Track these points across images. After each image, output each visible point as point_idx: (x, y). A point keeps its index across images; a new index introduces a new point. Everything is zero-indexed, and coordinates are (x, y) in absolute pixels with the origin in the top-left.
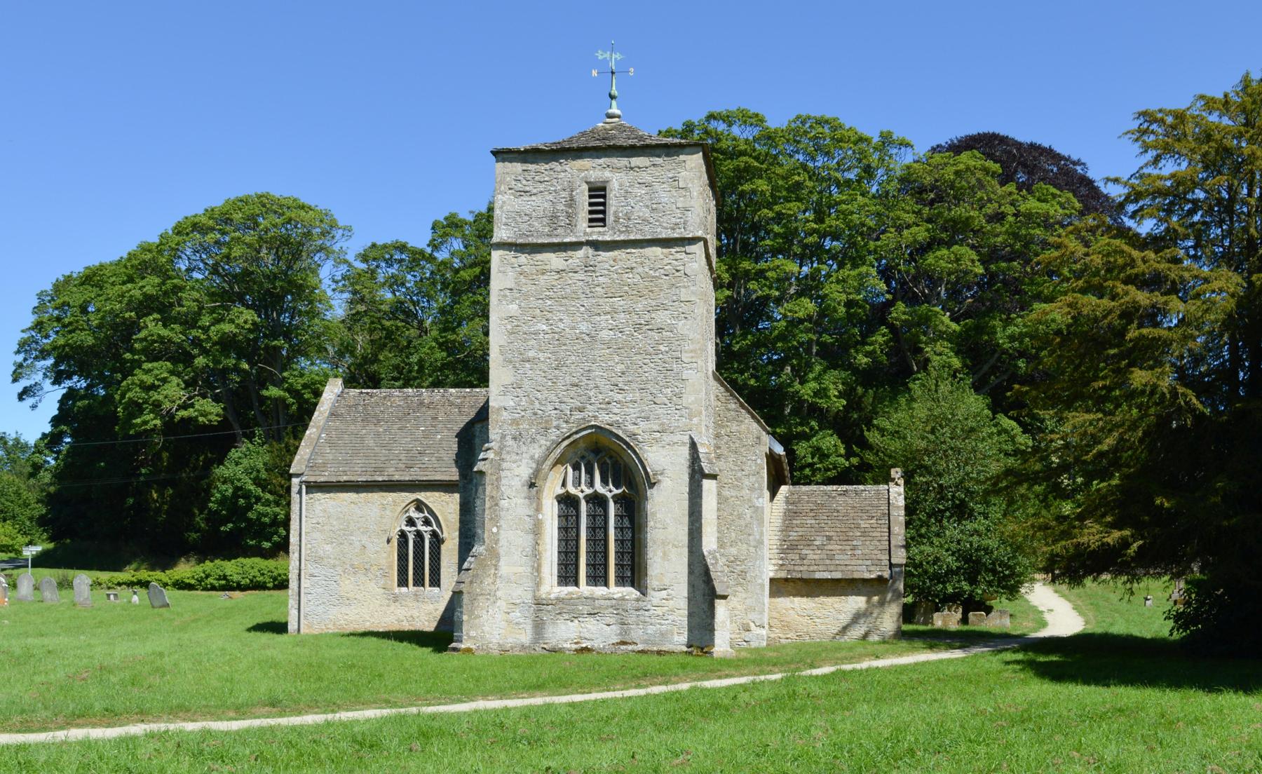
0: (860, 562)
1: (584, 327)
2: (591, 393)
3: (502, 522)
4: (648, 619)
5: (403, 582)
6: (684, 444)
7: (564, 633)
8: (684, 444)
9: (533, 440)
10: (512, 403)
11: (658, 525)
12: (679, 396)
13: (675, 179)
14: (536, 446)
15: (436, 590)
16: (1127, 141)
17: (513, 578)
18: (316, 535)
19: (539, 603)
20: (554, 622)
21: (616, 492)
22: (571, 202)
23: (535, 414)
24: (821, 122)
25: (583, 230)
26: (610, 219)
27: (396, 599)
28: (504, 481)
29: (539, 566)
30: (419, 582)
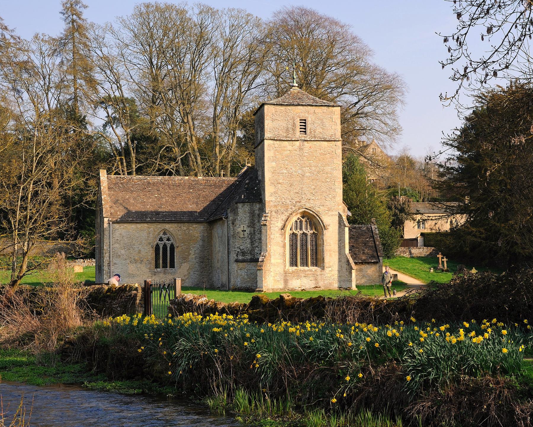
1: (300, 172)
5: (157, 266)
9: (283, 213)
12: (334, 197)
14: (284, 215)
18: (117, 245)
22: (294, 125)
25: (298, 134)
26: (308, 131)
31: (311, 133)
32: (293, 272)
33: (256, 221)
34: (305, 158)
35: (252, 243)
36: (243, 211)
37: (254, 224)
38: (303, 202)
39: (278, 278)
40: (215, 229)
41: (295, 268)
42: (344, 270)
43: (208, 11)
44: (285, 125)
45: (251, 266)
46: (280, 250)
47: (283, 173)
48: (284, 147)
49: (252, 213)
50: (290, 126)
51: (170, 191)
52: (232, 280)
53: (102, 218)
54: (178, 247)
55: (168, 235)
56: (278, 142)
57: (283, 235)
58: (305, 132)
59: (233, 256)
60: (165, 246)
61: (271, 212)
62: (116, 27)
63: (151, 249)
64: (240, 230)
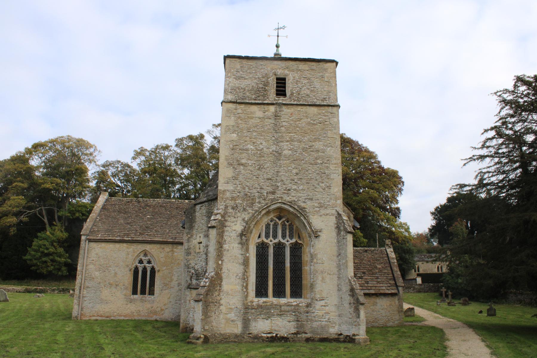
0: (382, 285)
2: (279, 184)
3: (224, 258)
4: (313, 319)
5: (135, 292)
6: (333, 215)
7: (261, 326)
8: (333, 215)
9: (244, 210)
10: (232, 188)
11: (318, 262)
12: (329, 187)
13: (323, 77)
14: (246, 213)
15: (152, 297)
16: (495, 100)
17: (230, 292)
18: (91, 266)
19: (247, 308)
20: (255, 320)
21: (291, 241)
22: (266, 84)
23: (247, 195)
26: (288, 93)
27: (131, 301)
28: (226, 234)
29: (247, 285)
30: (143, 292)
31: (292, 94)
32: (259, 306)
39: (232, 316)
42: (347, 305)
46: (239, 269)
47: (247, 150)
48: (251, 113)
54: (159, 271)
55: (149, 257)
56: (243, 106)
60: (145, 269)
63: (128, 272)
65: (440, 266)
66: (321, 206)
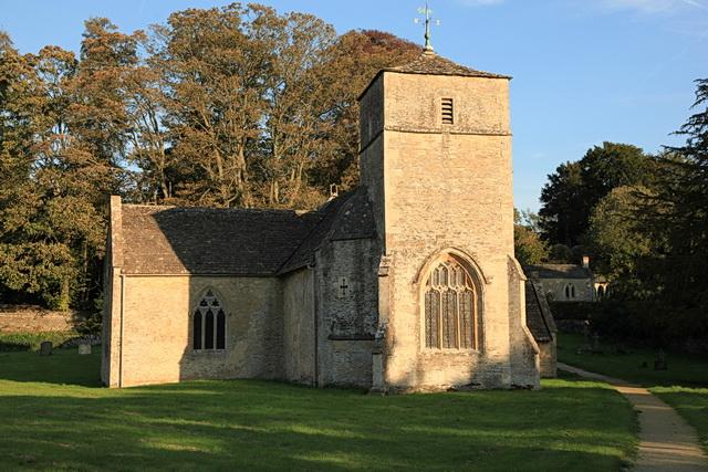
1: (442, 185)
18: (133, 312)
22: (433, 107)
24: (187, 13)
25: (439, 123)
26: (456, 119)
31: (460, 121)
33: (366, 270)
34: (451, 163)
35: (359, 307)
36: (343, 253)
37: (362, 276)
38: (449, 238)
40: (290, 287)
41: (435, 350)
43: (266, 19)
44: (417, 107)
45: (360, 348)
47: (414, 188)
49: (359, 258)
50: (426, 109)
51: (219, 229)
52: (322, 370)
53: (111, 269)
54: (230, 315)
57: (416, 292)
58: (451, 120)
59: (324, 330)
60: (210, 314)
61: (396, 253)
62: (150, 33)
64: (337, 285)
65: (570, 287)
66: (492, 250)
